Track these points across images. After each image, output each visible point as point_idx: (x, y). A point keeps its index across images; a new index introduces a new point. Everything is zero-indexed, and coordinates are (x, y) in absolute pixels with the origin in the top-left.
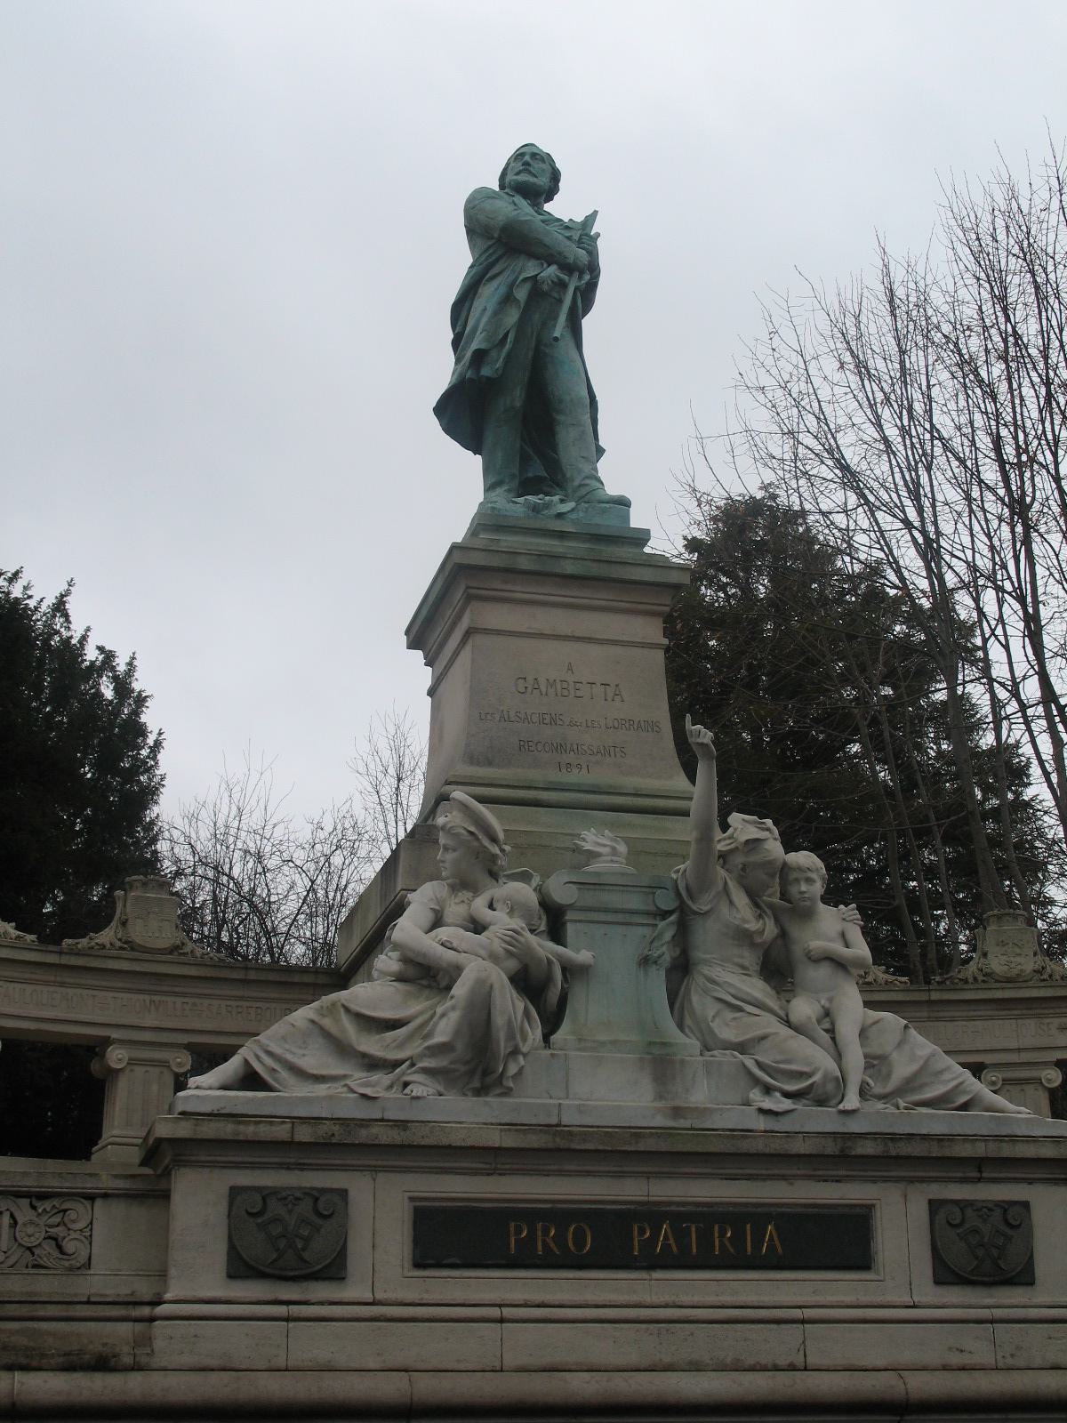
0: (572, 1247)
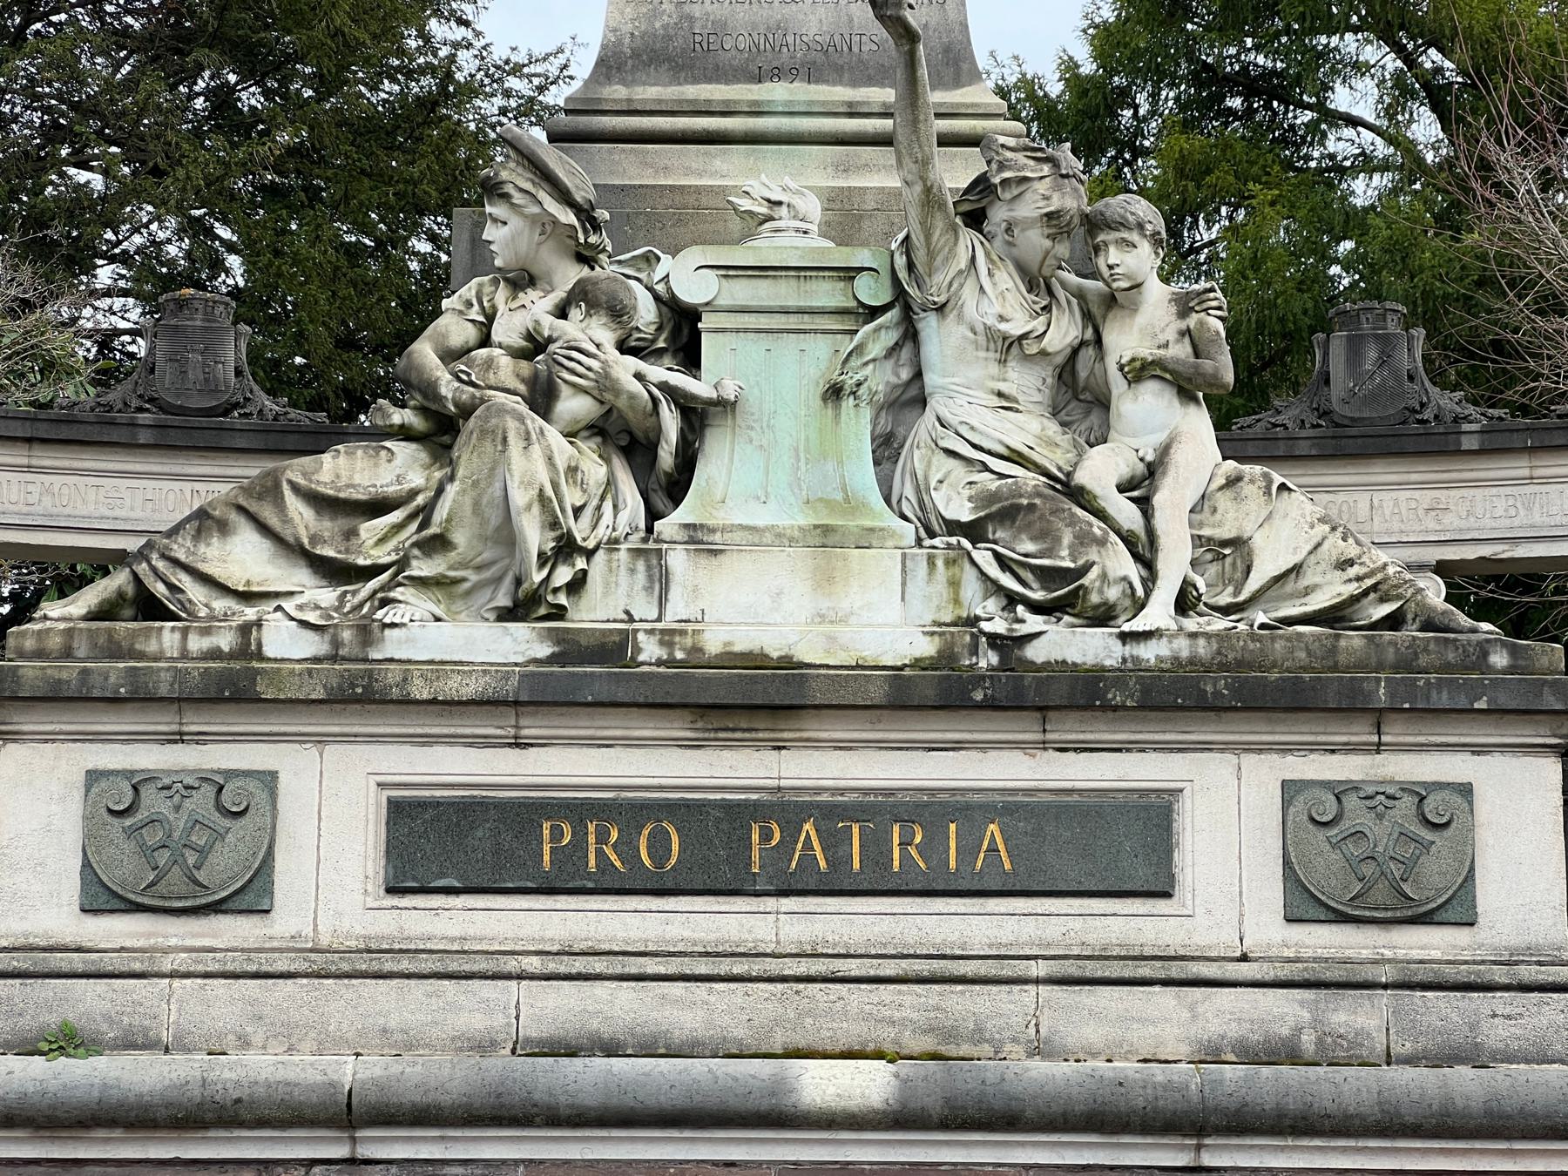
0: (647, 862)
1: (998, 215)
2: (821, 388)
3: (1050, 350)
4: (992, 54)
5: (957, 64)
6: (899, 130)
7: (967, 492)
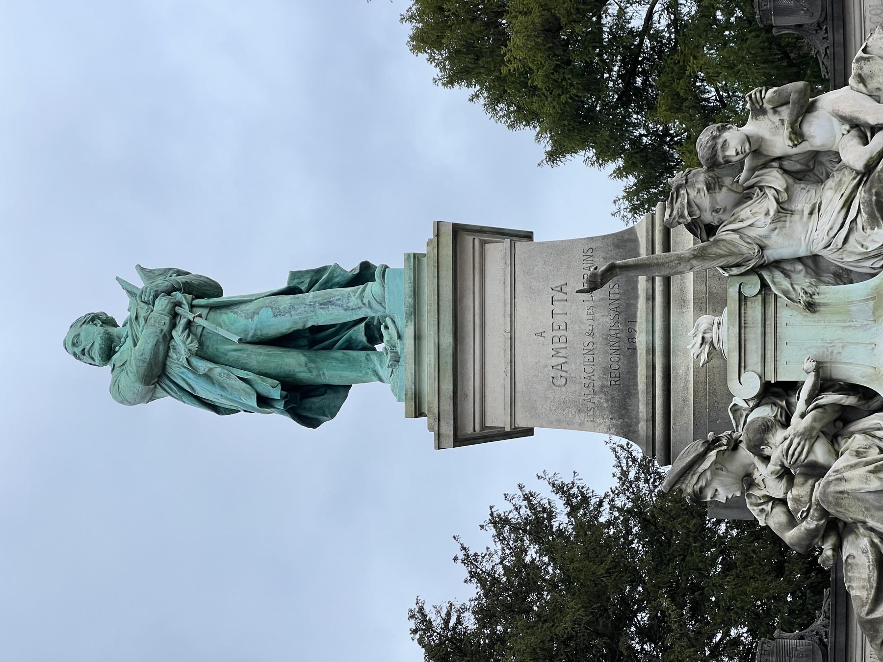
1: (709, 217)
2: (809, 314)
3: (785, 186)
4: (613, 215)
5: (624, 241)
6: (663, 273)
7: (869, 231)
